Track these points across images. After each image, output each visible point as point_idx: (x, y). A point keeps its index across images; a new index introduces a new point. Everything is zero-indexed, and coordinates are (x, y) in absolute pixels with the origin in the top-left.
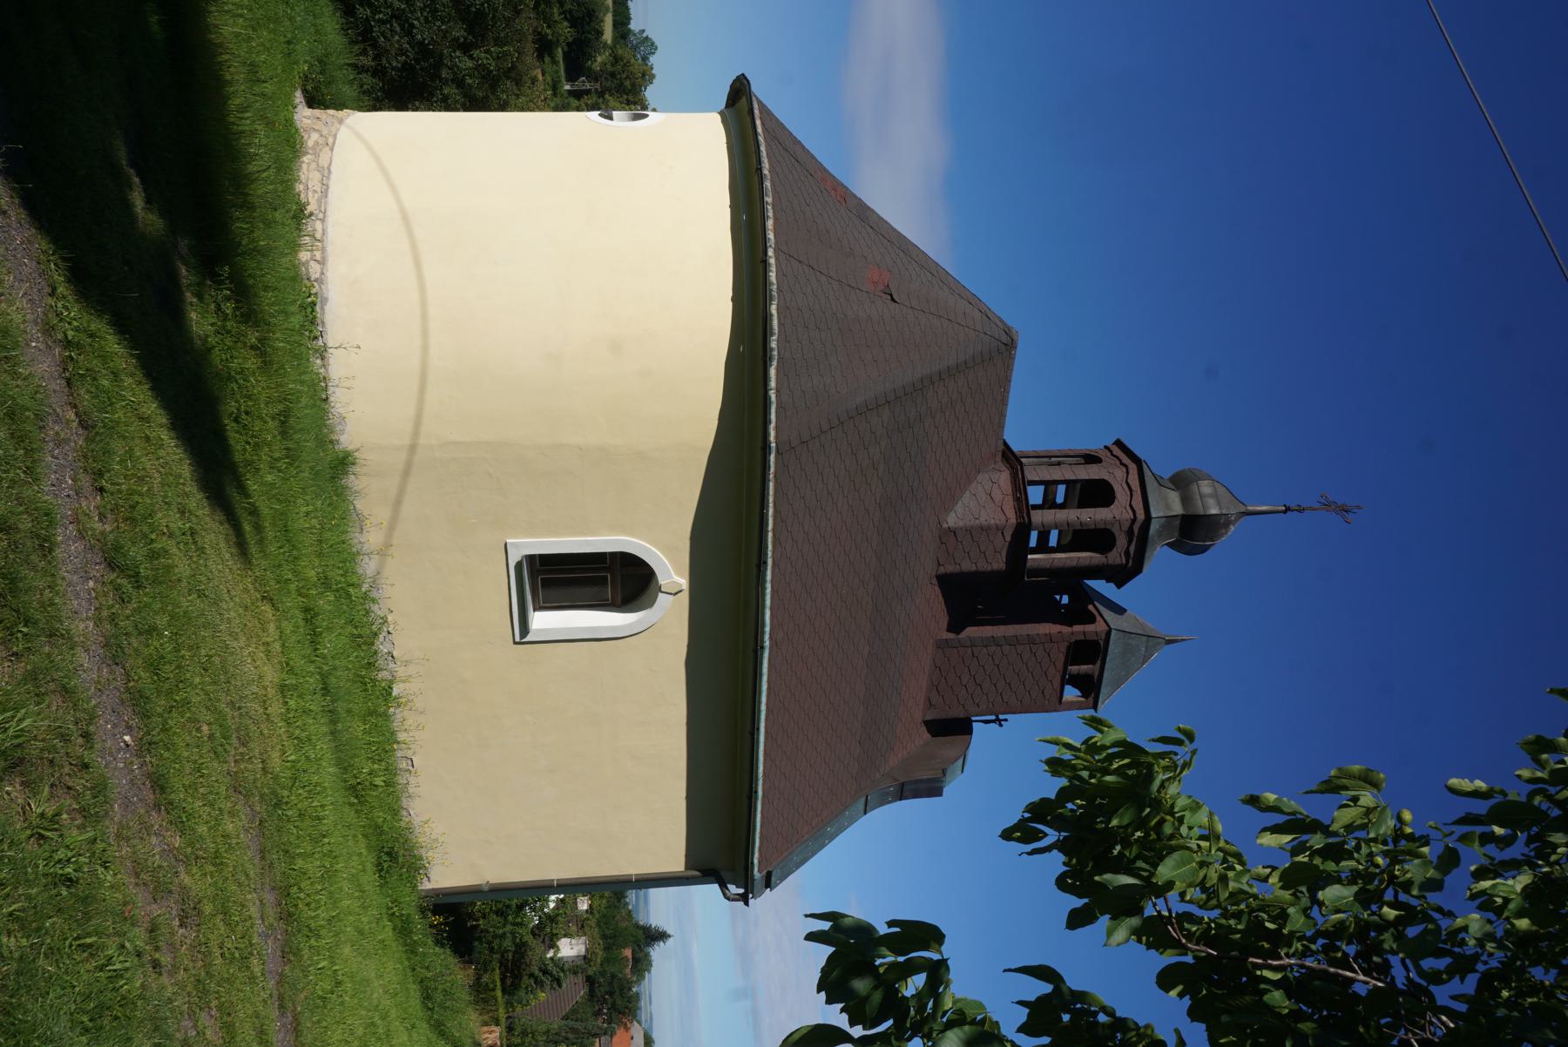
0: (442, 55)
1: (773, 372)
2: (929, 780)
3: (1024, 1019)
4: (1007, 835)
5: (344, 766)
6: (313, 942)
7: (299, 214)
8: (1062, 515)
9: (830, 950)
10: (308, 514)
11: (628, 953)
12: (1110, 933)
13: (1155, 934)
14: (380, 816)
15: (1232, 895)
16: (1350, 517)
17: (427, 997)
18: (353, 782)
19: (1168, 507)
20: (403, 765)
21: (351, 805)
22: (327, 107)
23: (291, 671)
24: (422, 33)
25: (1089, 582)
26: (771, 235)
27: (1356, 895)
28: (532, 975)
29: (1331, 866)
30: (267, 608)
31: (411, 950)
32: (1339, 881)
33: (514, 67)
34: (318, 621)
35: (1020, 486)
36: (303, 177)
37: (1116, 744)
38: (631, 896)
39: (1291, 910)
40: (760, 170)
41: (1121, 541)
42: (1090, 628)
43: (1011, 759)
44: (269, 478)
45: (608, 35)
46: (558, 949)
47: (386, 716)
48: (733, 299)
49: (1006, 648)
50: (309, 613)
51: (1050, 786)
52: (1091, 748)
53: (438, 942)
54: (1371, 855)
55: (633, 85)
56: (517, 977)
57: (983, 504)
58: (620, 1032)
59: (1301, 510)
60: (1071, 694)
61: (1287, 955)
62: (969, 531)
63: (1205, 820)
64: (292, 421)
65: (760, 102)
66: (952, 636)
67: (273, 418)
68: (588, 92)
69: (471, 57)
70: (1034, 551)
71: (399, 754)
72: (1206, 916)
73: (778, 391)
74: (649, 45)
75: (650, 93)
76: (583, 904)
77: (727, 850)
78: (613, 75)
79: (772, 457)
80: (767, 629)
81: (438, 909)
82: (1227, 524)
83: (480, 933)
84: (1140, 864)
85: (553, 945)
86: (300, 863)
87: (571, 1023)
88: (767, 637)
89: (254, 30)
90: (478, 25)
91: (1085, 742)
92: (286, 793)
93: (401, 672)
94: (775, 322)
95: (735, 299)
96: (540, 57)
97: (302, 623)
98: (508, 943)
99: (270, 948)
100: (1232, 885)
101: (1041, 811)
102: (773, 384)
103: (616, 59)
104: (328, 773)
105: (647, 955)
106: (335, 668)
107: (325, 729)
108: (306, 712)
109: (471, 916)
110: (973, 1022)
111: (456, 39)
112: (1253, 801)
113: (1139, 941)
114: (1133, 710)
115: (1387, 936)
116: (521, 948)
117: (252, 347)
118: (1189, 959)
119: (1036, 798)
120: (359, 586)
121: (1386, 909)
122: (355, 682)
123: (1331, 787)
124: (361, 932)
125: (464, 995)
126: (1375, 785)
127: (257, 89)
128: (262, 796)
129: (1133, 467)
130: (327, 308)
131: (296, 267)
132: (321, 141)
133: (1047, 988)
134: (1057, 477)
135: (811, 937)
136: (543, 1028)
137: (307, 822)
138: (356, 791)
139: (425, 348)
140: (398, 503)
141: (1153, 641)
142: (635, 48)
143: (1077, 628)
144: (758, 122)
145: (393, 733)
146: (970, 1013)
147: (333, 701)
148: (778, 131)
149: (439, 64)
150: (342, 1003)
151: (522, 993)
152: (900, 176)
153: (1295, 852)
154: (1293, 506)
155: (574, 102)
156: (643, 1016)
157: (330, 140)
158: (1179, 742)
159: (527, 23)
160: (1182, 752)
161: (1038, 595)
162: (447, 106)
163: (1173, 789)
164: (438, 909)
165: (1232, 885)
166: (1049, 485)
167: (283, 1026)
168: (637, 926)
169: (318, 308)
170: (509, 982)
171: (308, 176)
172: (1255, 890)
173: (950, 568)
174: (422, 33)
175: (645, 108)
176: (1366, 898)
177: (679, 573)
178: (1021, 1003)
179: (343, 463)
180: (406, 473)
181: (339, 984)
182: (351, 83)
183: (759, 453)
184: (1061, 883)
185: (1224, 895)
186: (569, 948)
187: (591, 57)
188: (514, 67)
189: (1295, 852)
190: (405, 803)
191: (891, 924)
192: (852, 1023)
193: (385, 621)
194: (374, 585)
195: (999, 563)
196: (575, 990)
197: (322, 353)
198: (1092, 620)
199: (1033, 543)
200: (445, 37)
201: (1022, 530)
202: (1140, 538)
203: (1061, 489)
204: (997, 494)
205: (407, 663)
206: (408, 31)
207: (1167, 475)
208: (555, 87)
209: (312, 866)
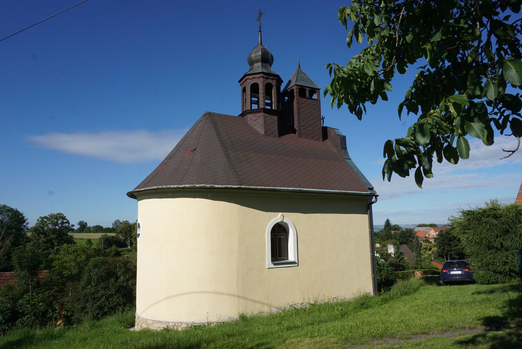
0: (119, 286)
1: (217, 186)
2: (341, 140)
3: (413, 114)
4: (360, 118)
5: (336, 319)
6: (389, 329)
7: (167, 330)
8: (261, 99)
9: (393, 172)
10: (258, 329)
11: (393, 232)
12: (388, 90)
13: (389, 75)
14: (351, 308)
15: (377, 52)
16: (263, 12)
17: (406, 294)
18: (340, 316)
19: (259, 67)
20: (335, 301)
21: (347, 317)
22: (135, 321)
23: (306, 334)
24: (112, 291)
25: (281, 90)
26: (175, 186)
27: (377, 15)
28: (399, 261)
29: (368, 22)
30: (287, 342)
31: (392, 298)
32: (373, 20)
33: (123, 263)
34: (291, 326)
35: (252, 111)
36: (156, 329)
37: (332, 87)
38: (375, 231)
39: (382, 34)
40: (156, 189)
41: (269, 81)
42: (295, 91)
43: (335, 116)
44: (247, 340)
45: (114, 234)
46: (391, 253)
47: (320, 305)
48: (195, 198)
49: (301, 116)
50: (289, 329)
51: (345, 106)
52: (333, 94)
53: (389, 290)
54: (365, 10)
55: (129, 227)
56: (400, 266)
57: (257, 123)
58: (417, 234)
59: (260, 27)
60: (315, 96)
61: (395, 35)
62: (265, 127)
63: (355, 60)
64: (230, 333)
65: (135, 189)
66: (297, 133)
67: (229, 339)
68: (131, 241)
69: (120, 277)
70: (272, 107)
71: (332, 302)
72: (383, 59)
73: (223, 185)
74: (117, 222)
75: (131, 222)
76: (378, 245)
77: (361, 201)
78: (126, 233)
79: (243, 187)
80: (294, 189)
81: (379, 290)
82: (265, 49)
83: (387, 276)
84: (368, 79)
85: (390, 254)
86: (365, 333)
87: (414, 250)
88: (297, 189)
89: (111, 343)
90: (110, 274)
91: (331, 95)
92: (344, 337)
93: (307, 301)
94: (202, 185)
95: (194, 197)
96: (121, 255)
97: (292, 331)
98: (389, 269)
99: (391, 342)
100: (374, 52)
101: (352, 109)
102: (220, 186)
103: (121, 232)
104: (338, 324)
105: (394, 226)
106: (305, 321)
107: (324, 324)
108: (319, 330)
109: (381, 280)
110: (415, 130)
111: (115, 281)
112: (349, 44)
113: (391, 80)
114: (323, 81)
115: (389, 5)
116: (391, 265)
117: (208, 345)
118: (396, 65)
119: (348, 110)
120: (280, 313)
121: (381, 6)
122: (310, 315)
123: (345, 22)
124: (386, 314)
125: (406, 282)
126: (344, 9)
127: (129, 342)
128: (345, 344)
129: (247, 77)
130: (195, 322)
131: (183, 331)
132: (145, 323)
133: (405, 108)
134: (250, 101)
135: (389, 180)
136: (415, 258)
137: (353, 330)
138: (343, 315)
139: (208, 292)
140: (255, 301)
141: (299, 71)
142: (118, 226)
143: (295, 94)
144: (141, 189)
145: (325, 303)
146: (412, 132)
147: (316, 322)
148: (144, 183)
149: (122, 286)
150: (408, 320)
151: (405, 264)
152: (157, 148)
153: (364, 32)
154: (259, 29)
155: (134, 245)
156: (412, 227)
157: (145, 320)
158: (331, 68)
159: (110, 259)
160: (334, 67)
161: (285, 107)
162: (135, 284)
163: (345, 70)
164: (379, 290)
165: (374, 52)
166: (252, 102)
167: (415, 338)
168: (385, 229)
169: (196, 325)
170: (401, 268)
171: (156, 327)
172: (376, 45)
173: (277, 133)
174: (112, 291)
175: (136, 224)
176: (378, 12)
177: (277, 216)
178: (408, 114)
179: (243, 318)
180: (246, 299)
181: (402, 321)
182: (127, 313)
183: (241, 191)
184: (374, 103)
185: (377, 55)
186: (391, 250)
187: (120, 240)
188: (123, 263)
189: (364, 32)
190: (347, 300)
191: (385, 156)
192: (415, 167)
193: (291, 306)
194: (280, 309)
195: (275, 118)
196: (404, 248)
197: (209, 324)
198: (293, 90)
199: (269, 108)
200: (114, 284)
201: (265, 111)
202: (268, 75)
203: (253, 99)
204: (254, 118)
205: (304, 299)
206: (112, 296)
207: (249, 67)
208: (129, 251)
209: (366, 329)
